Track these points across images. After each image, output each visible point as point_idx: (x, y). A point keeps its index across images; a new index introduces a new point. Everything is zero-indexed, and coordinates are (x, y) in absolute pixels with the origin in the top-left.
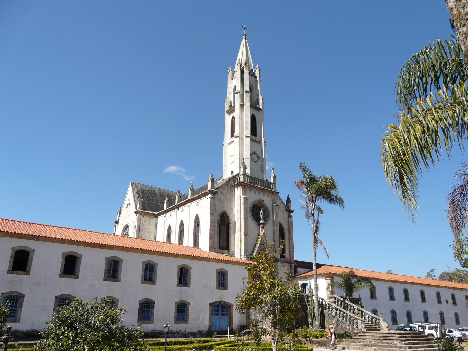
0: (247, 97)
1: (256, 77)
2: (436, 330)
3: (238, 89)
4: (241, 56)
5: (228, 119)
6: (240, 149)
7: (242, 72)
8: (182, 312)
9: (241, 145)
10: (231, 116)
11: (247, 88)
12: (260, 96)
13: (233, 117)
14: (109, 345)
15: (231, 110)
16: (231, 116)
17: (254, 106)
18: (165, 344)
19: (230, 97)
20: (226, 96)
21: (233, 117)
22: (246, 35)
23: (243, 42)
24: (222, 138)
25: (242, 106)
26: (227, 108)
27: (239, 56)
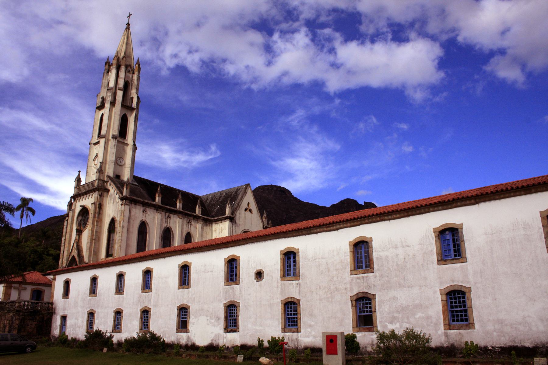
0: (120, 94)
3: (112, 84)
8: (460, 307)
11: (121, 83)
13: (103, 115)
21: (103, 115)
25: (113, 104)
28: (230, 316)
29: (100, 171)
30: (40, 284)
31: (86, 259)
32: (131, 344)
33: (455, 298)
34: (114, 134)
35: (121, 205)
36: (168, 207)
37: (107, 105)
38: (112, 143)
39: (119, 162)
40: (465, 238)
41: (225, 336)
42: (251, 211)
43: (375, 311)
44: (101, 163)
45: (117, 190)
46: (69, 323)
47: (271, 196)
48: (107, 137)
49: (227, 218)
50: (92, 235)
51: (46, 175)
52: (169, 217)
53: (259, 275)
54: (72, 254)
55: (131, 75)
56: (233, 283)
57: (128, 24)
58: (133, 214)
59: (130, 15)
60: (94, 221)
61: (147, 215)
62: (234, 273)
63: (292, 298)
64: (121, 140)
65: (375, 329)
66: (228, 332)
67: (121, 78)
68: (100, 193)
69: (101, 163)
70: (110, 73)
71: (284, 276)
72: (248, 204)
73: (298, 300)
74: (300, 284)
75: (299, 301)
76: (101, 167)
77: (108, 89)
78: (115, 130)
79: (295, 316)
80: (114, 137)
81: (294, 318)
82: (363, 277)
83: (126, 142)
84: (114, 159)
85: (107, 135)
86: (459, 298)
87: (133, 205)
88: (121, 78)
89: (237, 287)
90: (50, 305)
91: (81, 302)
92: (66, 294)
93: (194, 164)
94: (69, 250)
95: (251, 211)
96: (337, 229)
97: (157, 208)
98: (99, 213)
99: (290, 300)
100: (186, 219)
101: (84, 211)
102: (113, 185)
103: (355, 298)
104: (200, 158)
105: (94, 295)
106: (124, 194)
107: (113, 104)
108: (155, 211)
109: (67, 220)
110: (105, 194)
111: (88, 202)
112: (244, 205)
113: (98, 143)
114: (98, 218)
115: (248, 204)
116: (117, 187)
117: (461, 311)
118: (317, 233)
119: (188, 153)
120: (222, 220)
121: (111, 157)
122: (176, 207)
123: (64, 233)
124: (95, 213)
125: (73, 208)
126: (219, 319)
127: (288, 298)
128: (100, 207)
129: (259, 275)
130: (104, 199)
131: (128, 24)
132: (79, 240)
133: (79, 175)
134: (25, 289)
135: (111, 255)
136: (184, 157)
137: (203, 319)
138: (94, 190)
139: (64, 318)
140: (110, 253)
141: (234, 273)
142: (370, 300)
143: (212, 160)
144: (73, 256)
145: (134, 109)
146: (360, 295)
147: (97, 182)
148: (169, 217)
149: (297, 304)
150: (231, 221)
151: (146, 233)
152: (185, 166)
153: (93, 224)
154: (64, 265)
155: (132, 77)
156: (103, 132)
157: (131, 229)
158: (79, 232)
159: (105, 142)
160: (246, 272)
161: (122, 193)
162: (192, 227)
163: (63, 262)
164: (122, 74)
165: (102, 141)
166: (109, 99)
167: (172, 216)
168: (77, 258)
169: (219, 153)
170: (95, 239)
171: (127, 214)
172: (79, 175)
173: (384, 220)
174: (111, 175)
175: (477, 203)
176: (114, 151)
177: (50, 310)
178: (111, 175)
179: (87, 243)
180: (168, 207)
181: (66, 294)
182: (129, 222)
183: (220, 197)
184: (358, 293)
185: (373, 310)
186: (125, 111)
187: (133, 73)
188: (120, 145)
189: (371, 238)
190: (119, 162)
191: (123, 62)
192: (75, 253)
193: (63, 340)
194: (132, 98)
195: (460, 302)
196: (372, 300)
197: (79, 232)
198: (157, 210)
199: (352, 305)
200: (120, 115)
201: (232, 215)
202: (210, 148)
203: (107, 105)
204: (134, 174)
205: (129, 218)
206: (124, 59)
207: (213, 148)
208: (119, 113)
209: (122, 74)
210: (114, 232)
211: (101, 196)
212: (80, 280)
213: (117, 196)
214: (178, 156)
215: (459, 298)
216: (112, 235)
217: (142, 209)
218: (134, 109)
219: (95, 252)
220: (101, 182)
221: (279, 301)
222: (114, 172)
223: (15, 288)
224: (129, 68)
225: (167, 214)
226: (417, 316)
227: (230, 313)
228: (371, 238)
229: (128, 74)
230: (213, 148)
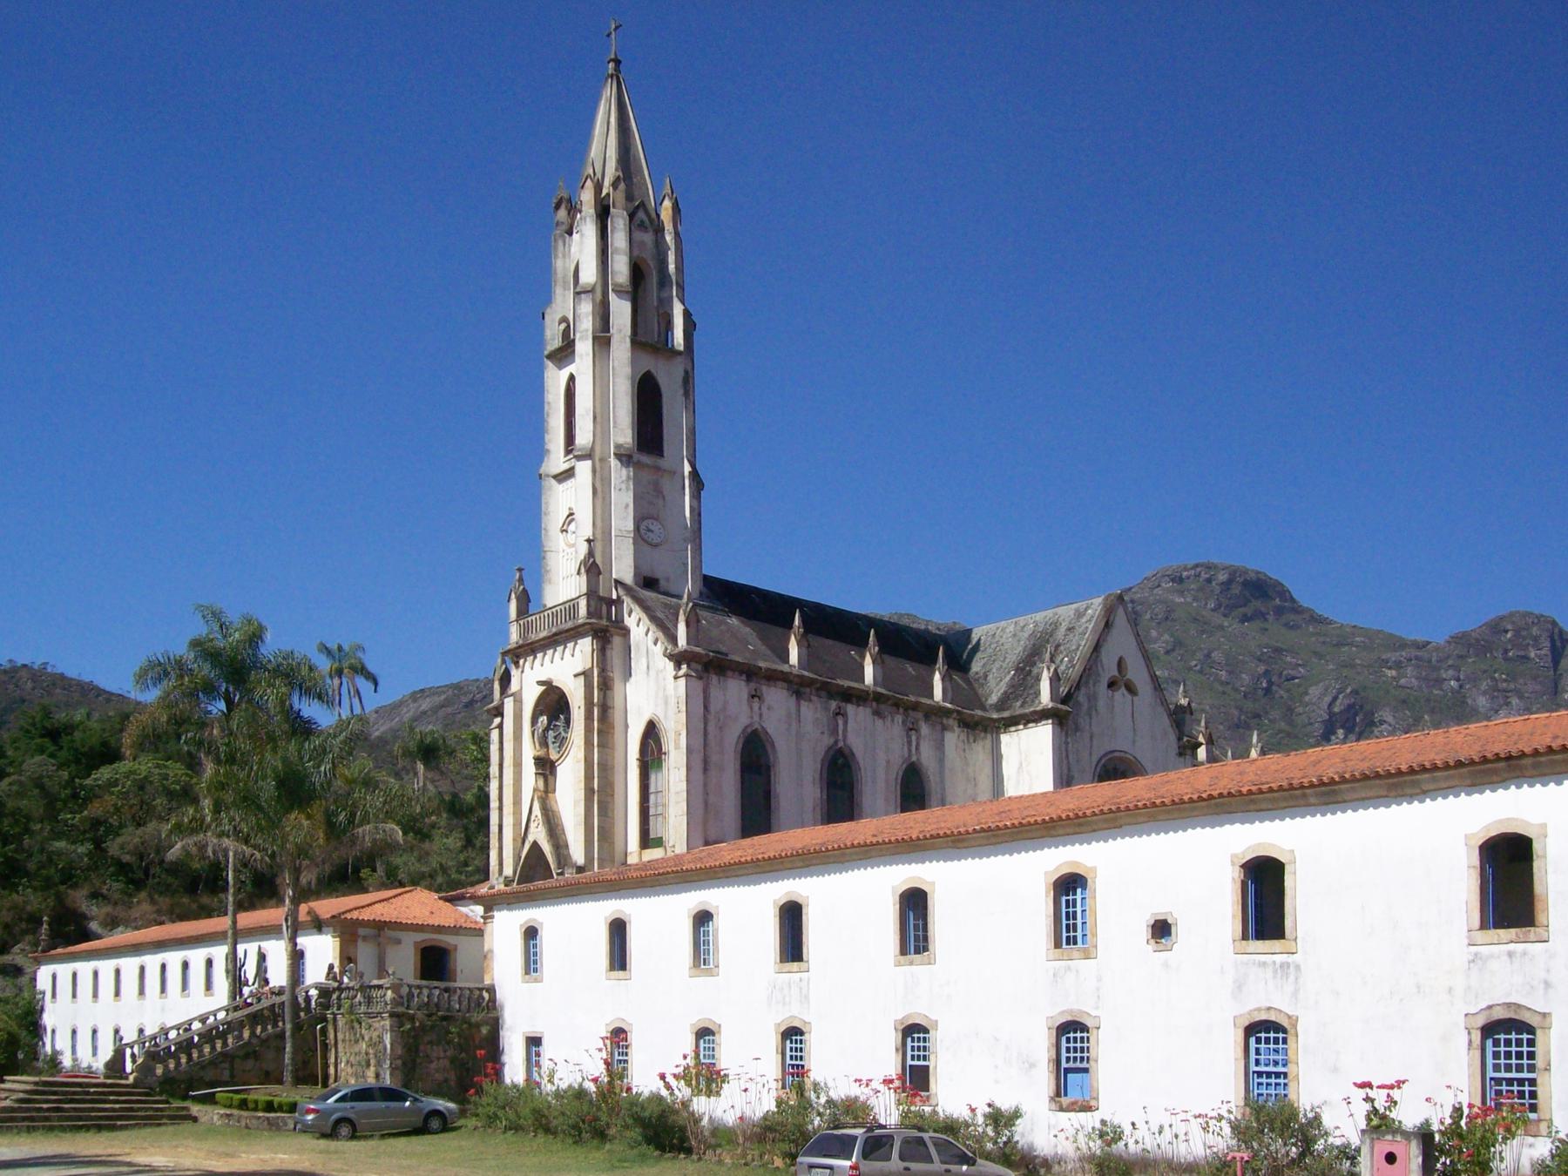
0: (621, 311)
1: (659, 230)
2: (800, 1090)
3: (589, 275)
4: (603, 148)
5: (555, 379)
6: (599, 512)
7: (603, 213)
8: (1519, 1068)
9: (600, 491)
10: (564, 375)
11: (621, 268)
12: (676, 301)
13: (572, 378)
14: (1275, 1160)
15: (565, 353)
16: (564, 375)
17: (649, 338)
18: (230, 908)
19: (563, 303)
20: (548, 300)
21: (572, 378)
22: (617, 62)
23: (609, 92)
24: (541, 453)
25: (602, 340)
26: (553, 341)
27: (595, 151)
28: (1068, 1059)
29: (592, 568)
30: (440, 929)
31: (577, 854)
32: (766, 1132)
33: (1508, 1043)
34: (621, 440)
35: (676, 678)
37: (584, 347)
38: (619, 475)
41: (1053, 1122)
42: (1131, 689)
43: (1547, 1069)
44: (589, 541)
45: (653, 628)
46: (548, 1051)
50: (589, 777)
52: (839, 713)
54: (531, 838)
56: (1076, 954)
63: (1269, 1009)
65: (1543, 1127)
66: (1061, 1109)
69: (589, 541)
70: (575, 236)
72: (1121, 664)
73: (1290, 1017)
74: (1298, 967)
75: (1295, 1021)
76: (591, 553)
77: (577, 294)
79: (1280, 1069)
81: (1278, 1075)
82: (1510, 954)
84: (630, 526)
86: (1519, 1043)
87: (714, 679)
90: (486, 995)
92: (531, 964)
94: (517, 823)
95: (1131, 689)
99: (1263, 1017)
101: (553, 704)
102: (638, 613)
103: (1481, 1021)
105: (621, 974)
106: (682, 641)
109: (500, 727)
113: (568, 474)
116: (653, 619)
117: (1521, 1082)
121: (623, 520)
122: (863, 680)
123: (494, 770)
125: (514, 687)
126: (1032, 1066)
127: (1259, 1010)
134: (399, 942)
135: (659, 843)
138: (573, 634)
140: (652, 836)
142: (1531, 1030)
144: (535, 845)
146: (1500, 1014)
147: (583, 603)
148: (839, 713)
149: (1285, 1031)
151: (768, 768)
154: (508, 871)
156: (584, 437)
157: (714, 758)
158: (546, 767)
160: (1116, 913)
161: (673, 639)
163: (504, 858)
164: (619, 239)
165: (584, 469)
166: (586, 325)
167: (850, 709)
168: (547, 848)
170: (601, 793)
176: (629, 498)
177: (486, 1006)
178: (628, 577)
179: (576, 803)
181: (531, 964)
184: (1490, 1007)
185: (1539, 1062)
186: (649, 363)
189: (1544, 826)
192: (538, 834)
195: (1519, 1055)
196: (1539, 1032)
197: (546, 767)
199: (1470, 1042)
200: (633, 378)
203: (584, 347)
204: (708, 570)
206: (622, 186)
208: (628, 370)
210: (660, 766)
212: (575, 927)
213: (659, 649)
215: (1519, 1043)
216: (653, 778)
222: (636, 567)
223: (365, 938)
224: (641, 215)
225: (833, 704)
227: (1068, 1050)
228: (1544, 826)
229: (638, 235)
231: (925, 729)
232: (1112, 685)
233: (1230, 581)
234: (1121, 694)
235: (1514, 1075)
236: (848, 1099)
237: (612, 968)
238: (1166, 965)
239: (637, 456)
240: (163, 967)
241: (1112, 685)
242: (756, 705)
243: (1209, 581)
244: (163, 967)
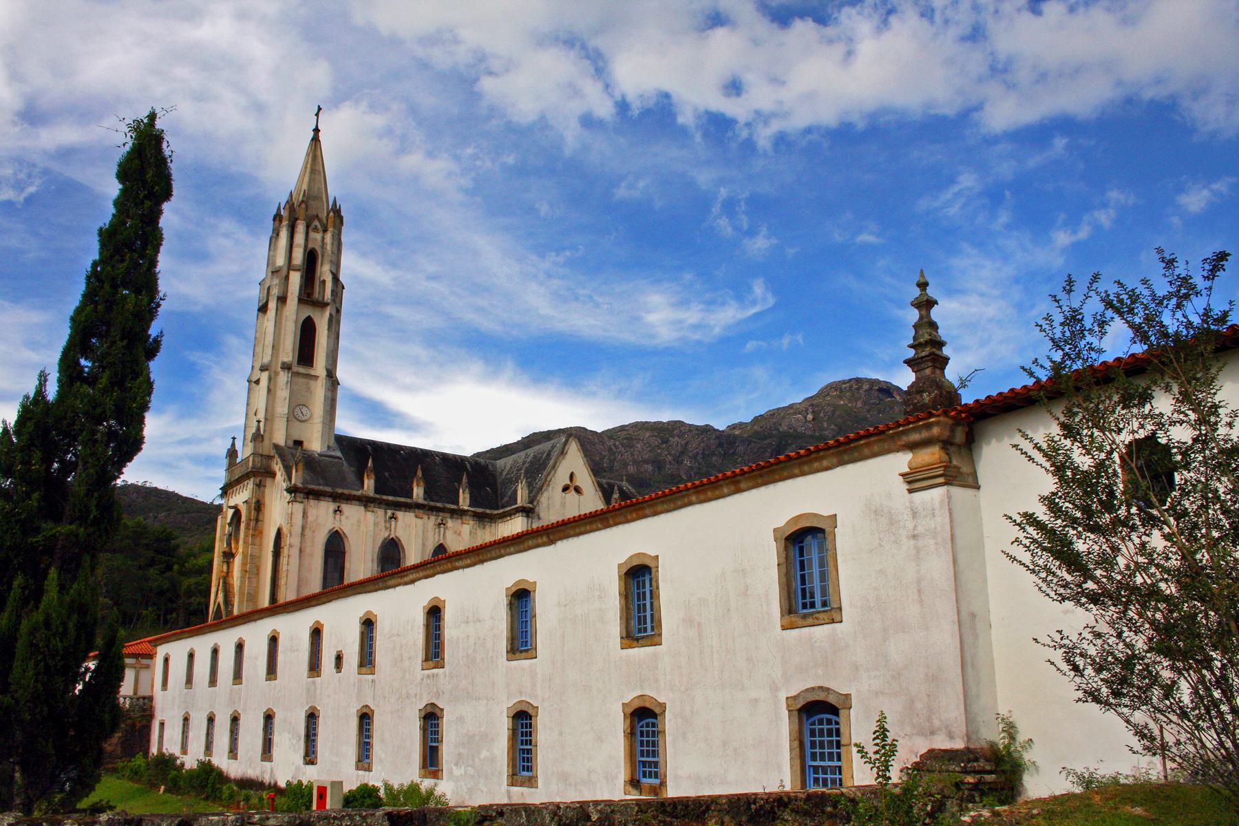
0: (296, 279)
11: (298, 256)
34: (286, 360)
36: (391, 498)
39: (296, 415)
40: (538, 611)
42: (578, 490)
47: (859, 404)
48: (273, 369)
49: (518, 510)
51: (407, 389)
52: (393, 517)
53: (339, 658)
55: (319, 236)
57: (317, 130)
58: (311, 518)
59: (320, 109)
60: (246, 536)
61: (343, 518)
62: (648, 614)
64: (302, 370)
67: (299, 246)
68: (258, 481)
71: (427, 660)
72: (572, 476)
78: (288, 352)
80: (286, 367)
83: (312, 372)
85: (273, 365)
88: (299, 246)
89: (318, 679)
91: (198, 695)
93: (717, 330)
95: (578, 490)
96: (413, 582)
97: (366, 502)
98: (257, 520)
99: (820, 696)
100: (433, 518)
104: (728, 315)
107: (282, 299)
108: (362, 508)
110: (269, 481)
111: (241, 497)
112: (561, 477)
114: (255, 529)
115: (572, 476)
118: (394, 586)
119: (701, 306)
120: (510, 514)
122: (411, 497)
124: (249, 520)
128: (258, 506)
129: (339, 658)
130: (267, 491)
131: (317, 130)
132: (228, 573)
133: (233, 445)
136: (692, 316)
137: (286, 735)
139: (162, 724)
141: (648, 614)
143: (757, 316)
145: (327, 304)
148: (393, 517)
150: (528, 517)
151: (344, 553)
152: (697, 336)
153: (245, 542)
155: (323, 238)
157: (308, 550)
159: (270, 379)
161: (290, 479)
162: (449, 534)
164: (299, 238)
167: (400, 514)
169: (771, 301)
170: (251, 570)
171: (298, 520)
172: (233, 445)
173: (457, 568)
174: (282, 442)
175: (552, 542)
180: (391, 498)
182: (303, 535)
183: (524, 463)
186: (307, 312)
187: (325, 231)
188: (301, 380)
190: (296, 415)
191: (301, 212)
193: (166, 763)
194: (324, 282)
198: (366, 506)
201: (531, 502)
202: (750, 289)
203: (272, 305)
205: (303, 528)
207: (759, 288)
209: (299, 238)
211: (260, 485)
214: (680, 315)
217: (332, 506)
218: (327, 304)
219: (253, 596)
220: (258, 459)
221: (355, 711)
225: (390, 513)
226: (482, 756)
230: (759, 288)
231: (450, 523)
232: (566, 489)
233: (871, 389)
234: (572, 494)
235: (827, 763)
236: (93, 789)
237: (427, 659)
238: (438, 695)
239: (296, 368)
240: (191, 656)
241: (566, 489)
242: (338, 517)
243: (858, 389)
244: (191, 656)
